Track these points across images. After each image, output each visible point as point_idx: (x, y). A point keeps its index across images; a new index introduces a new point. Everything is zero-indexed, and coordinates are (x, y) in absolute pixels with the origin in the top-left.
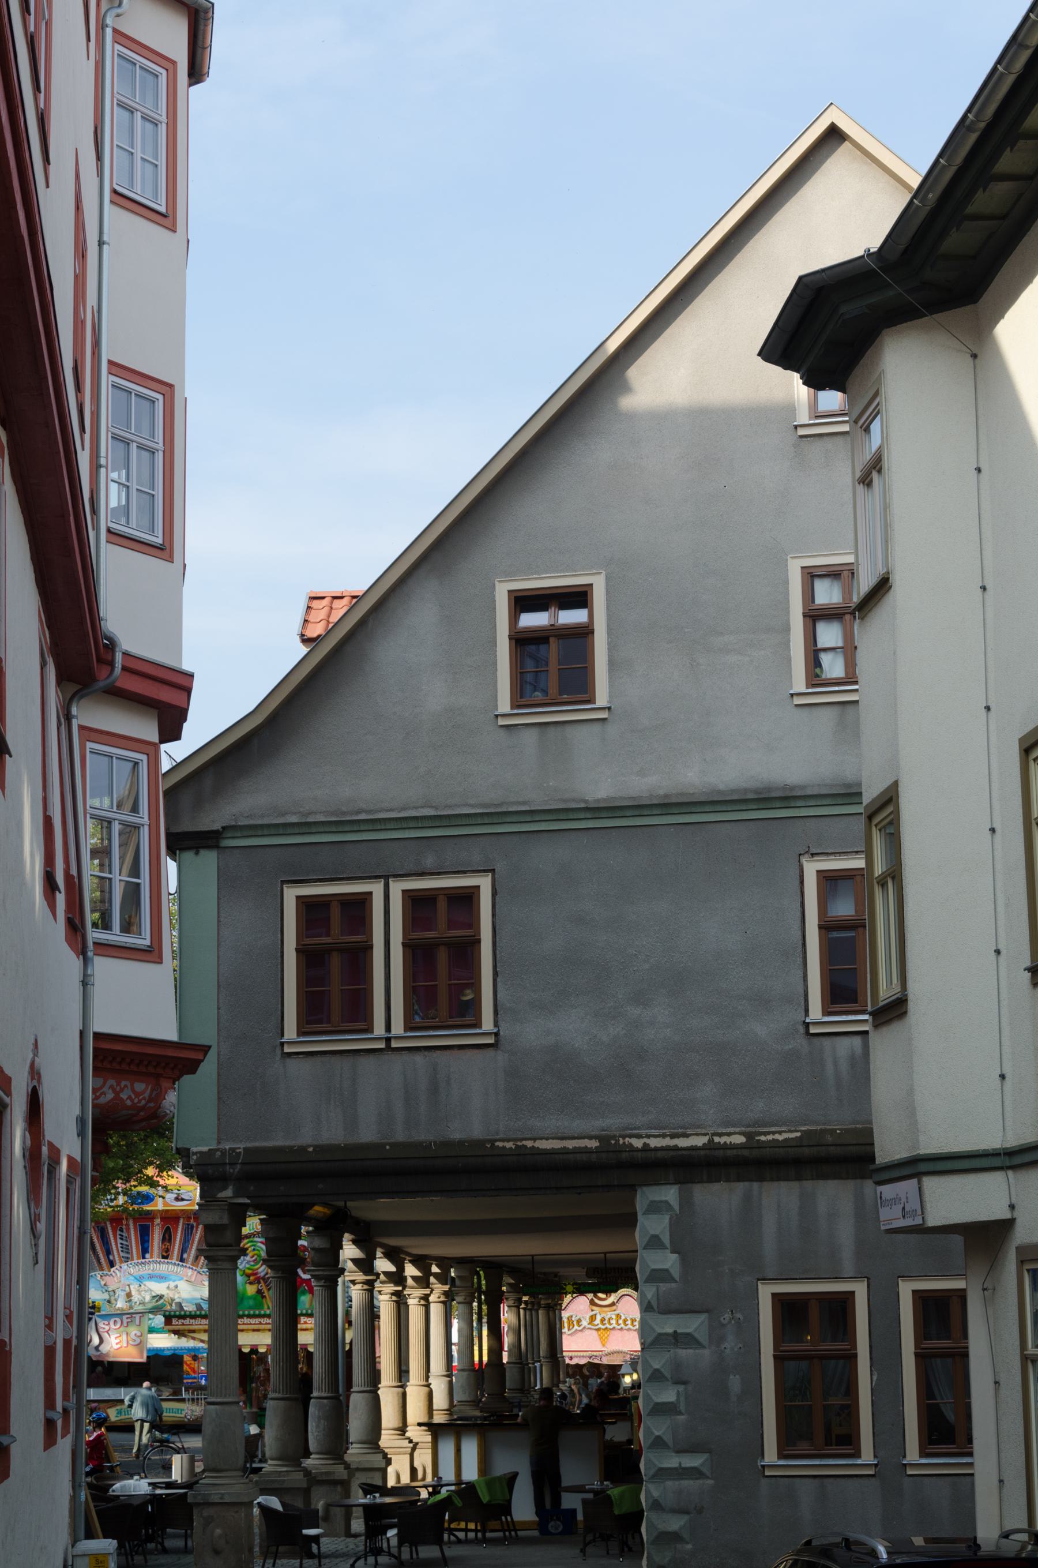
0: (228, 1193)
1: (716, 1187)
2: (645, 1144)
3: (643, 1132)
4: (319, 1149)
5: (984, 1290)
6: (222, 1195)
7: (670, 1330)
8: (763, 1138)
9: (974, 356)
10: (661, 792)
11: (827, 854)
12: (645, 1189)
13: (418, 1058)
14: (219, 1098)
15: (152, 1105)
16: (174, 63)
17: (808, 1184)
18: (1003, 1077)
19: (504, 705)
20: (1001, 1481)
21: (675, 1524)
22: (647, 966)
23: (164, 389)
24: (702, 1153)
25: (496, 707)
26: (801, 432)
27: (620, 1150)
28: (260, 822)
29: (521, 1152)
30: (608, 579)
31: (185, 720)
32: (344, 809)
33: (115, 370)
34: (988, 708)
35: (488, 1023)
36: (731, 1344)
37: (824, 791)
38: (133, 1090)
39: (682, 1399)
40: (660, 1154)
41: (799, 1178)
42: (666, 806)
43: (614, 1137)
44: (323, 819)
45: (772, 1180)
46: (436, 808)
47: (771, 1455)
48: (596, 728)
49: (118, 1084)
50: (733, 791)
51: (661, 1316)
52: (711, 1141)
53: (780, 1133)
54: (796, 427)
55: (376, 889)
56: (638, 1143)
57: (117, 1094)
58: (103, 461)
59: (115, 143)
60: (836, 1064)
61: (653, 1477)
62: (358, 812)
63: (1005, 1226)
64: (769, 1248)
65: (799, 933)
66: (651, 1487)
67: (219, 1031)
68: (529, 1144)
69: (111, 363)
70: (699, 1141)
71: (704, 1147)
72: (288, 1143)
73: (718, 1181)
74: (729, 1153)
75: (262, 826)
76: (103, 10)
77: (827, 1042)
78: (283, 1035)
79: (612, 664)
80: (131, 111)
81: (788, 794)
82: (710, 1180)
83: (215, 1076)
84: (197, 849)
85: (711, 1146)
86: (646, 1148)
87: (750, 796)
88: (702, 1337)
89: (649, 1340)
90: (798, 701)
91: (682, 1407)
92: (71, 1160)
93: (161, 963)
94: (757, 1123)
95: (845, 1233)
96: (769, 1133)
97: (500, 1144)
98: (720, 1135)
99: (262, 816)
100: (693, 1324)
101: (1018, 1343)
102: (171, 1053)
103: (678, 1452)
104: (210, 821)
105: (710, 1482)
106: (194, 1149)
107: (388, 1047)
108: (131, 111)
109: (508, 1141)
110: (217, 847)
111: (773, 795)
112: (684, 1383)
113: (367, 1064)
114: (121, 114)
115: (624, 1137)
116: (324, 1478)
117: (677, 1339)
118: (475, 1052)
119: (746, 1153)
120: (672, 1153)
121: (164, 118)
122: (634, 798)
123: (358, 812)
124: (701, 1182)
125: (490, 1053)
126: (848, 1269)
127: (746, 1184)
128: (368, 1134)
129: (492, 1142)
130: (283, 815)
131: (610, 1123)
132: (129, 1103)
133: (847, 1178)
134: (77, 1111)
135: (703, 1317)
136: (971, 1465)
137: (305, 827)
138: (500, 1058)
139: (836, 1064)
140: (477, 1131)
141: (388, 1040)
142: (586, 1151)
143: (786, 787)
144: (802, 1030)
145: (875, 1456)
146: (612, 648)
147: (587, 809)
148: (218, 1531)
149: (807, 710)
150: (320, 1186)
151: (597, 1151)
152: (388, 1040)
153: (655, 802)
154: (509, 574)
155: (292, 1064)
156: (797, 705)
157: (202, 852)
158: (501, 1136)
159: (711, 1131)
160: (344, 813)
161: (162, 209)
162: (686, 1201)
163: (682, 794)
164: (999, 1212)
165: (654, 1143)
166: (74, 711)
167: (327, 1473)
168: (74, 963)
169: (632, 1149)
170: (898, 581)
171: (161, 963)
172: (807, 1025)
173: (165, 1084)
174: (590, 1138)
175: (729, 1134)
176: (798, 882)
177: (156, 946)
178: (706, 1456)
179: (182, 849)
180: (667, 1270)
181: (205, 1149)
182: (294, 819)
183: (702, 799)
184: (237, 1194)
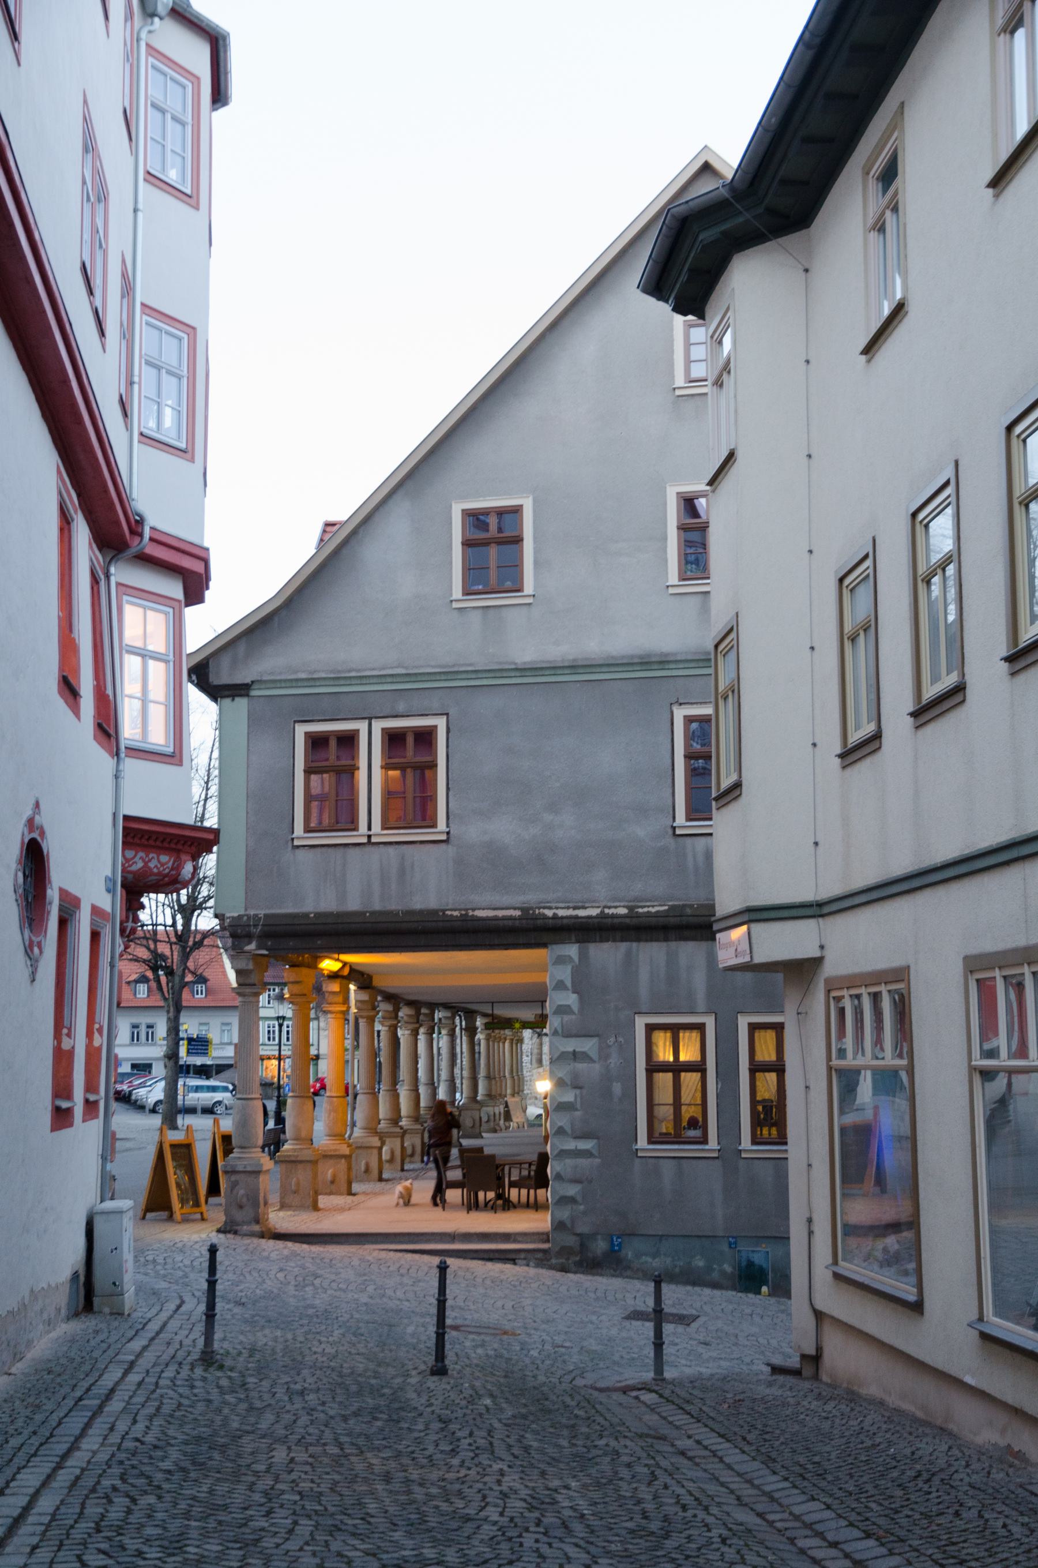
0: (252, 947)
1: (606, 946)
2: (555, 914)
3: (553, 905)
4: (318, 915)
5: (798, 1014)
6: (248, 948)
7: (571, 1049)
8: (640, 910)
9: (806, 271)
10: (571, 657)
11: (692, 704)
12: (554, 946)
13: (391, 850)
14: (247, 878)
15: (174, 872)
16: (198, 78)
17: (673, 944)
18: (816, 844)
19: (457, 592)
20: (810, 1165)
21: (572, 1190)
22: (558, 785)
23: (189, 330)
24: (596, 920)
25: (451, 595)
26: (678, 392)
27: (536, 918)
28: (279, 678)
29: (464, 918)
30: (535, 501)
31: (208, 588)
32: (340, 668)
33: (147, 311)
34: (814, 745)
35: (442, 825)
36: (614, 1061)
37: (690, 657)
38: (159, 861)
39: (579, 1099)
40: (565, 921)
41: (666, 939)
42: (574, 668)
43: (531, 908)
44: (323, 675)
45: (646, 941)
46: (406, 668)
47: (642, 1142)
48: (525, 609)
49: (147, 856)
50: (623, 657)
51: (565, 1040)
52: (602, 912)
53: (653, 906)
54: (674, 389)
55: (362, 726)
56: (549, 913)
57: (146, 864)
58: (136, 379)
59: (149, 136)
60: (694, 857)
61: (556, 1156)
62: (350, 671)
63: (816, 963)
64: (644, 991)
65: (670, 761)
66: (555, 1163)
67: (247, 829)
68: (471, 913)
69: (143, 304)
70: (594, 912)
71: (597, 917)
72: (296, 911)
73: (607, 941)
74: (616, 921)
75: (280, 681)
76: (136, 28)
77: (689, 841)
78: (293, 833)
79: (536, 563)
80: (163, 111)
81: (664, 659)
82: (601, 941)
83: (244, 862)
84: (233, 697)
85: (602, 915)
86: (555, 917)
87: (636, 660)
88: (594, 1054)
89: (556, 1056)
90: (671, 591)
91: (578, 1106)
92: (96, 910)
93: (181, 765)
94: (636, 899)
95: (699, 982)
96: (645, 907)
97: (449, 913)
98: (609, 908)
99: (280, 674)
100: (588, 1046)
101: (824, 1055)
102: (187, 833)
103: (576, 1138)
104: (242, 677)
105: (598, 1161)
106: (228, 915)
107: (369, 842)
108: (163, 111)
109: (455, 910)
110: (248, 695)
111: (653, 660)
112: (581, 1088)
113: (352, 852)
114: (154, 115)
115: (539, 908)
116: (332, 1153)
117: (575, 1056)
118: (431, 846)
119: (628, 920)
120: (573, 921)
121: (189, 120)
122: (548, 662)
123: (350, 671)
124: (595, 941)
125: (443, 846)
126: (701, 1006)
127: (628, 943)
128: (353, 904)
129: (444, 911)
130: (296, 672)
131: (530, 898)
132: (155, 870)
133: (701, 940)
134: (108, 872)
135: (595, 1040)
136: (786, 1151)
137: (312, 681)
138: (450, 850)
139: (694, 857)
140: (431, 902)
141: (369, 837)
142: (511, 918)
143: (662, 654)
144: (670, 832)
145: (719, 1143)
146: (537, 551)
147: (516, 669)
148: (242, 1192)
149: (678, 597)
150: (319, 942)
151: (520, 918)
152: (369, 837)
153: (566, 664)
154: (463, 497)
155: (301, 854)
156: (672, 594)
157: (237, 699)
158: (450, 907)
159: (602, 904)
160: (339, 672)
161: (188, 191)
162: (583, 956)
163: (587, 659)
164: (811, 951)
165: (561, 913)
166: (112, 570)
167: (335, 1150)
168: (109, 762)
169: (545, 917)
170: (740, 455)
171: (181, 765)
172: (674, 828)
173: (184, 857)
174: (515, 909)
175: (616, 907)
176: (669, 724)
177: (177, 752)
178: (595, 1141)
179: (222, 697)
180: (569, 1006)
181: (236, 915)
182: (303, 676)
183: (601, 662)
184: (259, 947)
